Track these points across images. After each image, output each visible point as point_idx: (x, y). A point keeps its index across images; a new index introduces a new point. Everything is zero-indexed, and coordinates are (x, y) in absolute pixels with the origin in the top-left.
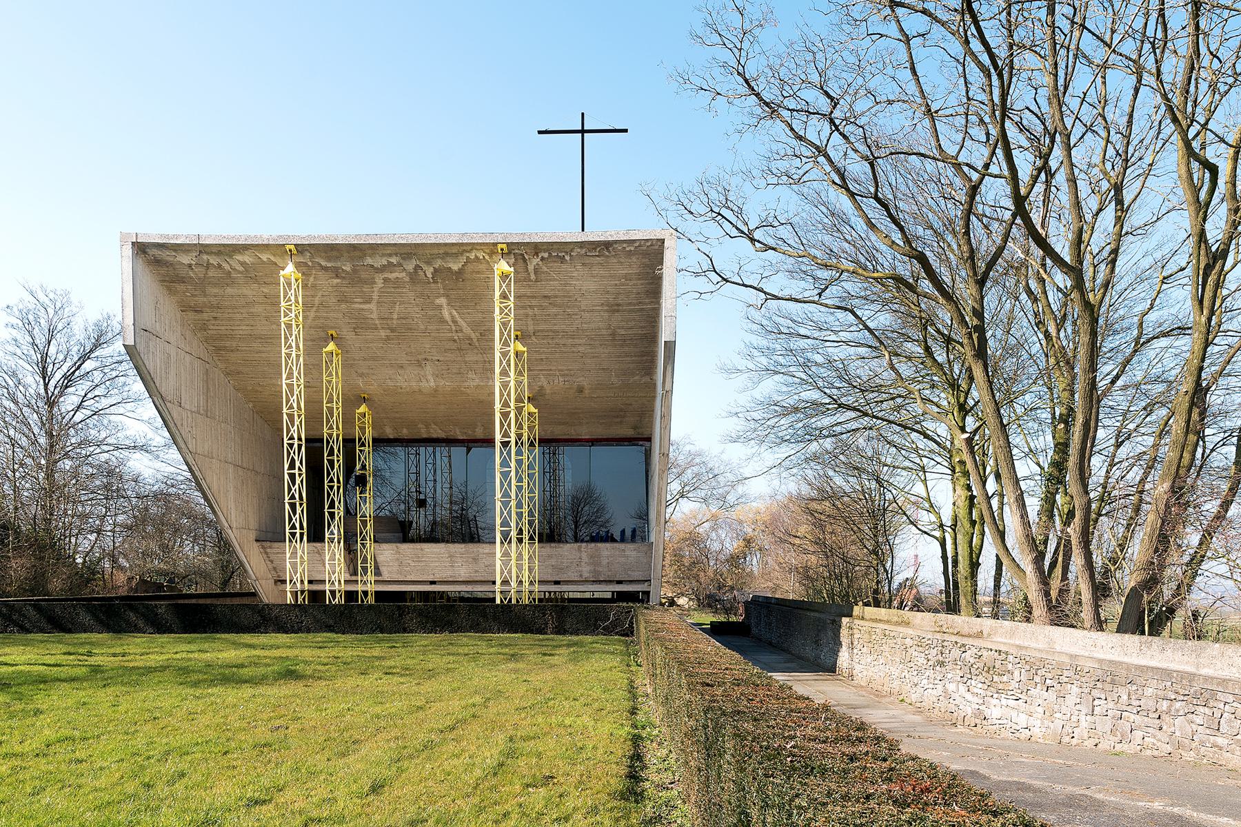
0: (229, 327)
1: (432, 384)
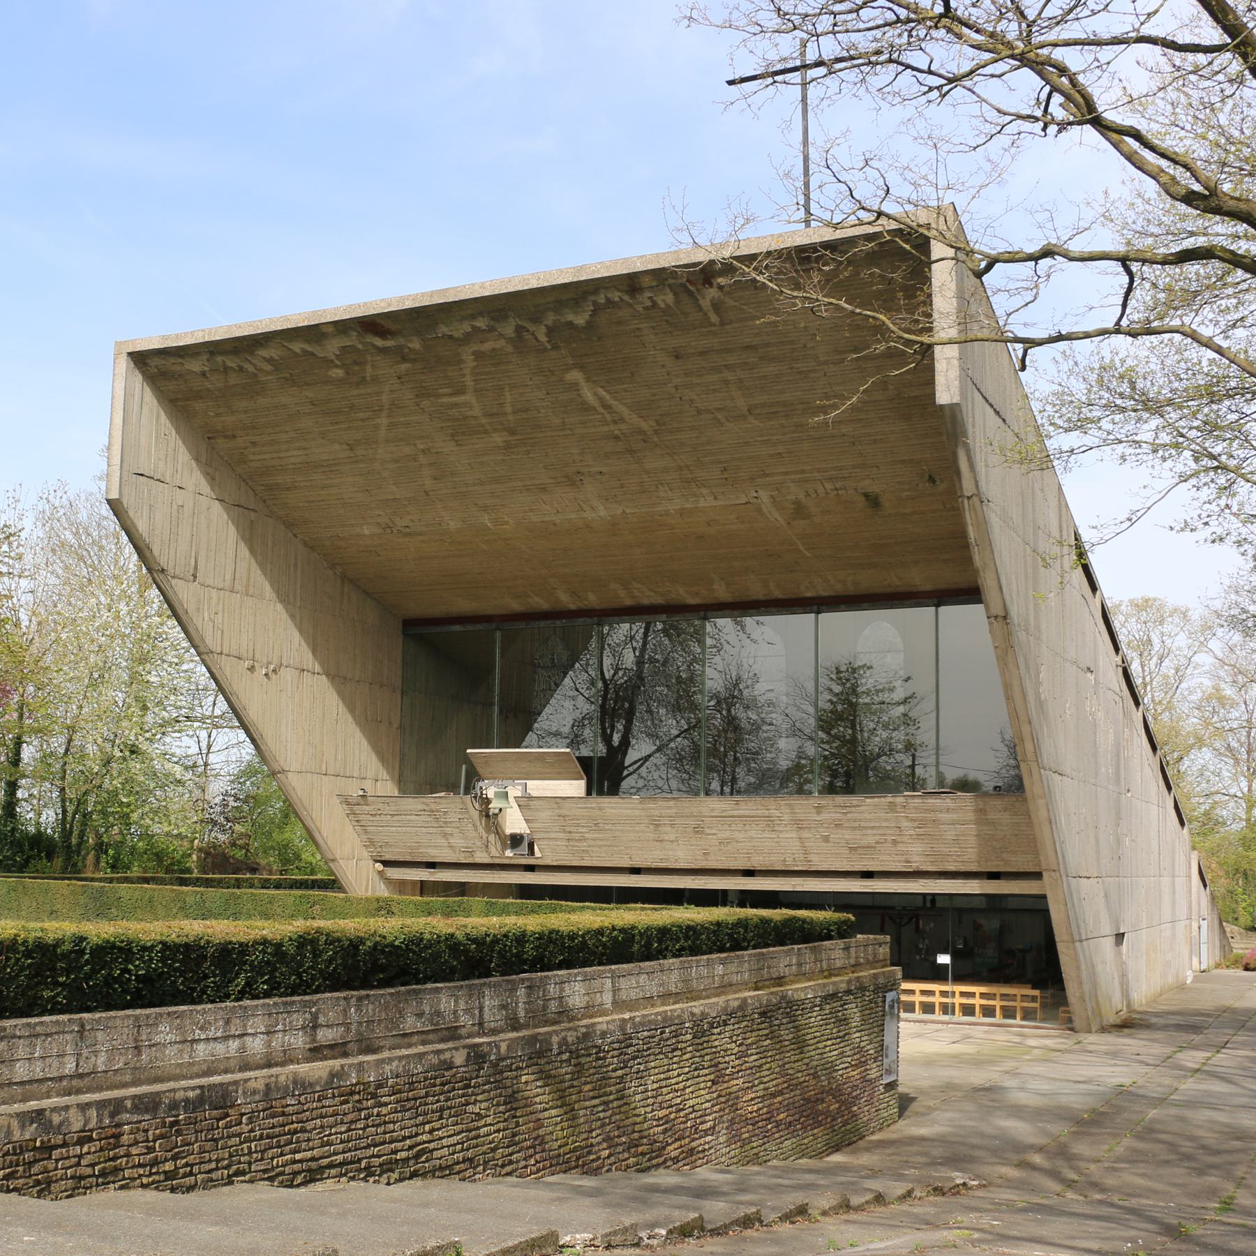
0: (275, 455)
1: (603, 513)
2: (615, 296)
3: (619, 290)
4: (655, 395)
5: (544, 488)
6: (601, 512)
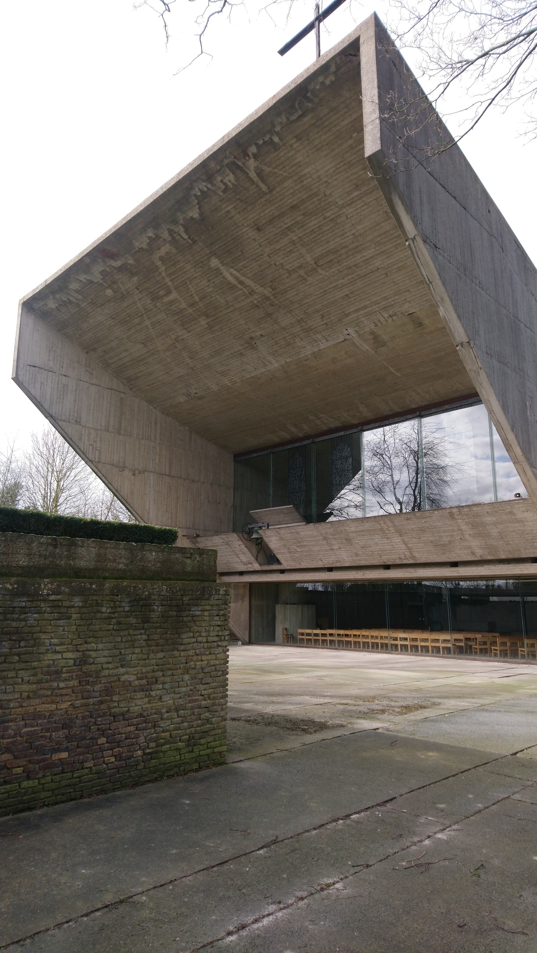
1: (276, 365)
2: (203, 186)
3: (203, 181)
4: (260, 266)
5: (241, 353)
6: (275, 364)
